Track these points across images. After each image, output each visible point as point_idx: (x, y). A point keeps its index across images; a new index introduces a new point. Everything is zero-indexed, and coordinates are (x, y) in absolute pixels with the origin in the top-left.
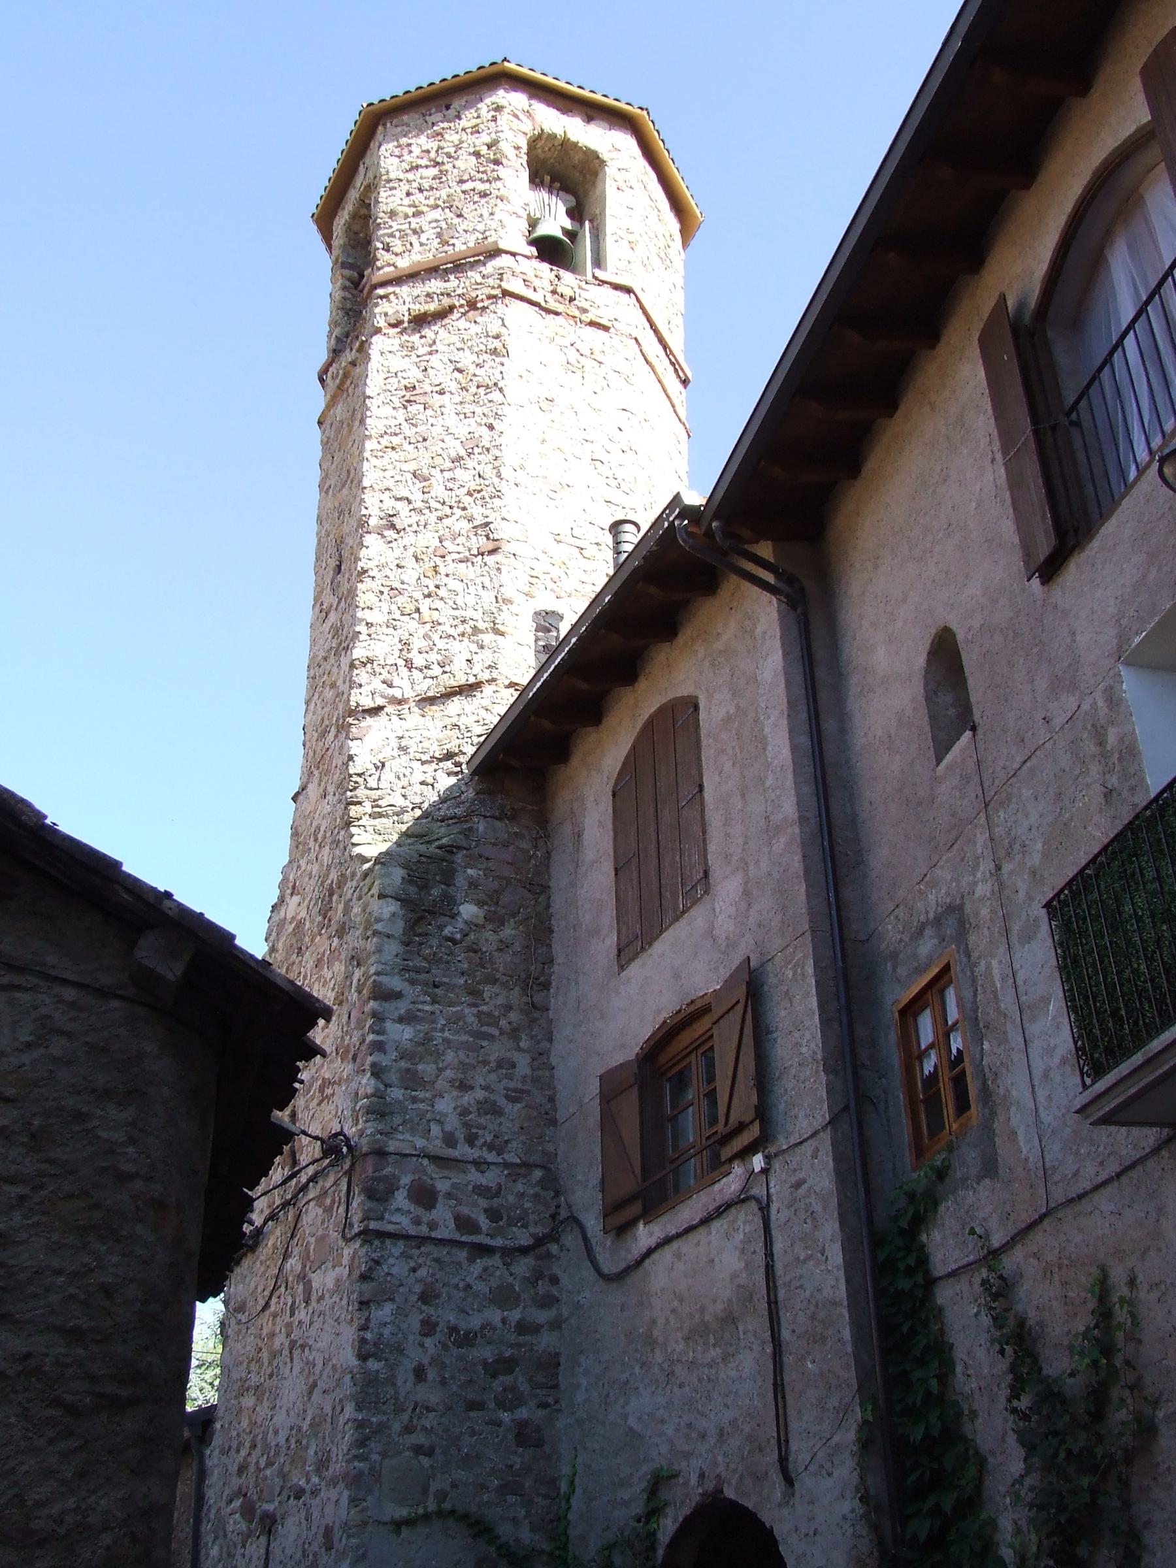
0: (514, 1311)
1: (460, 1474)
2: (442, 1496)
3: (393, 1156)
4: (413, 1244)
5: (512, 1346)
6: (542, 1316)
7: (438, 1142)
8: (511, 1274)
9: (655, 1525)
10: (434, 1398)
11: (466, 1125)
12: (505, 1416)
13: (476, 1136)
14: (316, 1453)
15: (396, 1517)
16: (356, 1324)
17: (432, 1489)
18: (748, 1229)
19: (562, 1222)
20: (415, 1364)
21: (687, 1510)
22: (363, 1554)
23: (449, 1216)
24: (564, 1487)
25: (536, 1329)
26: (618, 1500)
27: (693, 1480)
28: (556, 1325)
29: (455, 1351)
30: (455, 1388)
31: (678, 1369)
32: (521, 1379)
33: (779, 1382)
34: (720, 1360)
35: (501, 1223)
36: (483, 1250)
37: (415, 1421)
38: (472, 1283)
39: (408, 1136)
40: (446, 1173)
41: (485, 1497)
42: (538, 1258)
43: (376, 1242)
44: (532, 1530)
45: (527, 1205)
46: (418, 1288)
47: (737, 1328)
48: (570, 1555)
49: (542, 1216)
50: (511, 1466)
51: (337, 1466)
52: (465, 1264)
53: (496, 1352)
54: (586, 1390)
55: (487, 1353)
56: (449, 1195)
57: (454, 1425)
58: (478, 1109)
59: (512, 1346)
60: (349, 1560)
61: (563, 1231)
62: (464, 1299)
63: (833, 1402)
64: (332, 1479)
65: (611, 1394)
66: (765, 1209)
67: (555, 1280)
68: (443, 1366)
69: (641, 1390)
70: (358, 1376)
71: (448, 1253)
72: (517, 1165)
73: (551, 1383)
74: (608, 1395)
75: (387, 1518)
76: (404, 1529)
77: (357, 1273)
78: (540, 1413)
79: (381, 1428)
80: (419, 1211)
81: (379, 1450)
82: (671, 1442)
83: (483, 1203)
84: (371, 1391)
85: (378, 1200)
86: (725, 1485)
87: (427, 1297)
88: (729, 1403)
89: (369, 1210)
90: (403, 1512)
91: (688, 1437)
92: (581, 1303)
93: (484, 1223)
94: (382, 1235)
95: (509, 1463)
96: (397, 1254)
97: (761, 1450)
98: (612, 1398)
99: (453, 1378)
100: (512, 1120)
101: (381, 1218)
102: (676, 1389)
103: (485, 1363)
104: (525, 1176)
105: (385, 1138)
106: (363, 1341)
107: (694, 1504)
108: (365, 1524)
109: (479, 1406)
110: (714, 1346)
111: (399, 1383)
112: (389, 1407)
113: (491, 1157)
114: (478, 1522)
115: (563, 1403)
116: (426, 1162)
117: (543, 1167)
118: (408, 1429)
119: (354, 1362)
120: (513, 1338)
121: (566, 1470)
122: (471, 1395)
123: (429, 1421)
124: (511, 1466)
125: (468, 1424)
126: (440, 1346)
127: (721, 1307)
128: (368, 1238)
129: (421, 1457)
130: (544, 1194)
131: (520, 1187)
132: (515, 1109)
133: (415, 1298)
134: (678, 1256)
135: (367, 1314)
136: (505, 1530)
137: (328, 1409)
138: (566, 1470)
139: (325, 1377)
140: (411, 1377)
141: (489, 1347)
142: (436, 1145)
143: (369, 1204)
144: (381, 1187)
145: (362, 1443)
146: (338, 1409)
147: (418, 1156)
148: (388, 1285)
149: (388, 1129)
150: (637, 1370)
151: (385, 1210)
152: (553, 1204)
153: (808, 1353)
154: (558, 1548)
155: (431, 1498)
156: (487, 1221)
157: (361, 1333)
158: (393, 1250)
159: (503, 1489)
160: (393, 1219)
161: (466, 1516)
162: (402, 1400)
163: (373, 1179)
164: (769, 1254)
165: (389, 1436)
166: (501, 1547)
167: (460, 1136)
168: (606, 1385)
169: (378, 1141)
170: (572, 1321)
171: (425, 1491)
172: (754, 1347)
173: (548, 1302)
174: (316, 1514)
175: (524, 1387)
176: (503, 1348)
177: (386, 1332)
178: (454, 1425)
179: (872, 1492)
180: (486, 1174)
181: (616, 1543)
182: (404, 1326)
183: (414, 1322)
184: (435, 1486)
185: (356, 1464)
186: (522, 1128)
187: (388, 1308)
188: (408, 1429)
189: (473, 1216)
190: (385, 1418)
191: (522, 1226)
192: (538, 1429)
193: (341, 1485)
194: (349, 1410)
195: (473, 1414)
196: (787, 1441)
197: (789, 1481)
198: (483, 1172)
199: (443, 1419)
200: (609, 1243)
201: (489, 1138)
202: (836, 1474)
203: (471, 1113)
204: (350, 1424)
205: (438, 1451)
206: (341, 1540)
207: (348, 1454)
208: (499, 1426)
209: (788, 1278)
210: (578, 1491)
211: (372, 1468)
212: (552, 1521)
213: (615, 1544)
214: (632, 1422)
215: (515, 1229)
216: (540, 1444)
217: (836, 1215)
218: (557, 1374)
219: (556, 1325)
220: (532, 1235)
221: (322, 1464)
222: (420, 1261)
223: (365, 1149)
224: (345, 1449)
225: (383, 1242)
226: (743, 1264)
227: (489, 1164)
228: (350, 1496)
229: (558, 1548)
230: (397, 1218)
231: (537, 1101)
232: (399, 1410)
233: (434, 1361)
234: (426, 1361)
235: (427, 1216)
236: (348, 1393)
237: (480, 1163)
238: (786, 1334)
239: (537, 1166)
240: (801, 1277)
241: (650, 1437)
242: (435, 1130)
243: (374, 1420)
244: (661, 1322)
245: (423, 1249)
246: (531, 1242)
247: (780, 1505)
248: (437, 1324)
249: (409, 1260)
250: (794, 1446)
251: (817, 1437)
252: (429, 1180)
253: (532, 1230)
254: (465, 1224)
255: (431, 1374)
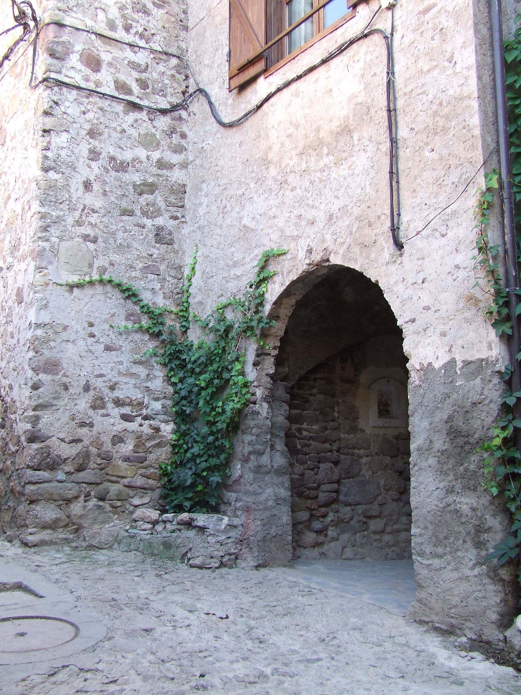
0: (155, 152)
1: (116, 258)
2: (103, 270)
3: (68, 28)
4: (84, 94)
5: (154, 175)
6: (175, 159)
7: (103, 25)
8: (154, 127)
9: (265, 290)
10: (98, 203)
11: (124, 16)
12: (148, 223)
13: (131, 26)
14: (10, 242)
15: (70, 281)
16: (40, 147)
17: (96, 265)
18: (369, 57)
19: (191, 95)
20: (85, 179)
21: (294, 277)
22: (46, 305)
23: (110, 78)
24: (187, 271)
25: (170, 166)
26: (232, 276)
27: (302, 254)
28: (184, 166)
29: (113, 173)
30: (113, 199)
31: (291, 178)
32: (159, 198)
33: (394, 171)
34: (332, 165)
35: (147, 90)
36: (135, 107)
37: (84, 217)
38: (126, 129)
39: (80, 16)
40: (109, 48)
41: (133, 274)
42: (173, 119)
43: (56, 89)
44: (164, 298)
45: (167, 82)
46: (87, 126)
47: (352, 137)
48: (191, 315)
49: (176, 91)
50: (152, 255)
51: (24, 249)
52: (121, 114)
53: (142, 178)
54: (207, 206)
55: (137, 178)
56: (110, 64)
57: (112, 224)
58: (133, 8)
59: (154, 175)
60: (34, 309)
61: (191, 102)
62: (120, 139)
63: (454, 177)
64: (22, 256)
65: (228, 206)
66: (388, 40)
67: (184, 136)
68: (105, 183)
69: (255, 198)
70: (41, 182)
71: (109, 105)
72: (160, 52)
73: (180, 204)
74: (225, 207)
75: (64, 283)
76: (75, 289)
77: (41, 110)
78: (172, 222)
79: (58, 221)
80: (89, 71)
81: (57, 235)
82: (282, 231)
83: (135, 75)
84: (52, 193)
85: (57, 58)
86: (332, 254)
87: (92, 134)
88: (340, 195)
89: (50, 65)
90: (74, 279)
91: (297, 225)
92: (205, 148)
93: (135, 88)
94: (60, 84)
95: (150, 253)
96: (71, 100)
97: (370, 225)
98: (229, 208)
99: (111, 192)
100: (158, 21)
101: (60, 72)
102: (288, 193)
103: (135, 186)
104: (165, 61)
105: (63, 14)
106: (46, 157)
107: (300, 272)
108: (47, 284)
109: (130, 213)
110: (327, 155)
111: (72, 190)
112: (65, 206)
113: (142, 43)
114: (128, 290)
115: (188, 218)
116: (93, 37)
117: (178, 57)
118: (78, 223)
119: (39, 174)
120: (154, 170)
121: (189, 261)
122: (124, 204)
123: (94, 219)
124: (152, 255)
125: (122, 224)
126: (102, 169)
127: (338, 124)
128: (50, 85)
129: (88, 243)
130: (178, 76)
131: (161, 68)
132: (160, 13)
133: (84, 133)
134: (297, 94)
135: (48, 139)
136: (146, 297)
137: (19, 211)
138: (189, 261)
139: (16, 190)
140: (82, 188)
141: (138, 174)
142: (102, 28)
143: (50, 60)
144: (59, 49)
145: (45, 229)
146: (27, 208)
147: (89, 32)
148: (65, 121)
149: (64, 7)
150: (252, 185)
151: (63, 66)
152: (184, 84)
153: (427, 144)
154: (182, 311)
155: (95, 271)
156: (138, 88)
157: (44, 152)
158: (68, 96)
159: (146, 269)
160: (69, 74)
161: (119, 285)
162: (75, 203)
163: (54, 42)
164: (391, 72)
165: (65, 226)
166: (143, 307)
167: (119, 23)
168: (224, 200)
169: (57, 15)
170: (197, 162)
171: (91, 266)
172: (368, 148)
173: (179, 150)
174: (10, 281)
175: (162, 205)
176: (148, 176)
177: (63, 153)
178: (112, 224)
179: (491, 245)
180: (138, 55)
181: (230, 304)
182: (76, 151)
183: (84, 149)
184: (97, 263)
185: (40, 243)
186: (164, 28)
187: (65, 136)
188: (78, 223)
189: (127, 82)
190: (62, 213)
191: (162, 95)
192: (170, 234)
193: (29, 259)
194: (36, 206)
195: (125, 218)
196: (399, 215)
197: (399, 246)
198: (135, 53)
199: (104, 219)
200: (230, 101)
201: (141, 30)
202: (451, 234)
203: (127, 8)
204: (36, 216)
205: (100, 240)
206: (29, 295)
207: (34, 237)
208: (143, 227)
209: (409, 89)
210: (198, 274)
211: (52, 247)
212: (178, 293)
213: (225, 307)
214: (246, 221)
215: (157, 97)
216: (170, 243)
217: (471, 23)
218: (184, 198)
219: (184, 166)
220: (170, 103)
221: (15, 248)
222: (89, 107)
223: (47, 21)
224: (32, 234)
225: (61, 89)
226: (362, 86)
227: (140, 47)
228: (35, 266)
229: (182, 311)
230: (72, 73)
231: (175, 11)
232: (72, 209)
233: (97, 177)
234: (92, 178)
235: (94, 77)
236: (34, 195)
237: (134, 46)
238: (403, 132)
239: (174, 56)
240: (423, 85)
241: (262, 230)
242: (101, 15)
243: (54, 213)
244: (276, 148)
245: (91, 99)
246: (168, 107)
247: (387, 264)
248: (100, 154)
249: (80, 106)
250: (405, 218)
251: (432, 208)
252: (96, 51)
253: (169, 99)
254: (121, 86)
255: (96, 187)
